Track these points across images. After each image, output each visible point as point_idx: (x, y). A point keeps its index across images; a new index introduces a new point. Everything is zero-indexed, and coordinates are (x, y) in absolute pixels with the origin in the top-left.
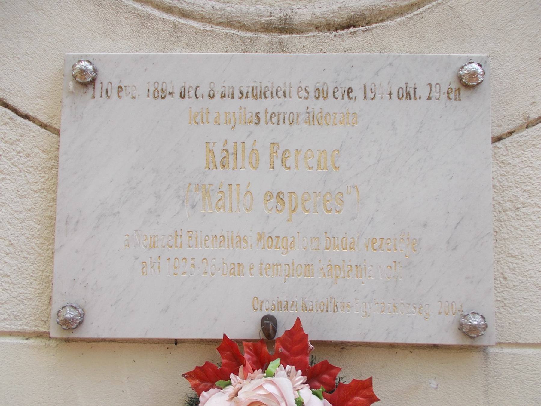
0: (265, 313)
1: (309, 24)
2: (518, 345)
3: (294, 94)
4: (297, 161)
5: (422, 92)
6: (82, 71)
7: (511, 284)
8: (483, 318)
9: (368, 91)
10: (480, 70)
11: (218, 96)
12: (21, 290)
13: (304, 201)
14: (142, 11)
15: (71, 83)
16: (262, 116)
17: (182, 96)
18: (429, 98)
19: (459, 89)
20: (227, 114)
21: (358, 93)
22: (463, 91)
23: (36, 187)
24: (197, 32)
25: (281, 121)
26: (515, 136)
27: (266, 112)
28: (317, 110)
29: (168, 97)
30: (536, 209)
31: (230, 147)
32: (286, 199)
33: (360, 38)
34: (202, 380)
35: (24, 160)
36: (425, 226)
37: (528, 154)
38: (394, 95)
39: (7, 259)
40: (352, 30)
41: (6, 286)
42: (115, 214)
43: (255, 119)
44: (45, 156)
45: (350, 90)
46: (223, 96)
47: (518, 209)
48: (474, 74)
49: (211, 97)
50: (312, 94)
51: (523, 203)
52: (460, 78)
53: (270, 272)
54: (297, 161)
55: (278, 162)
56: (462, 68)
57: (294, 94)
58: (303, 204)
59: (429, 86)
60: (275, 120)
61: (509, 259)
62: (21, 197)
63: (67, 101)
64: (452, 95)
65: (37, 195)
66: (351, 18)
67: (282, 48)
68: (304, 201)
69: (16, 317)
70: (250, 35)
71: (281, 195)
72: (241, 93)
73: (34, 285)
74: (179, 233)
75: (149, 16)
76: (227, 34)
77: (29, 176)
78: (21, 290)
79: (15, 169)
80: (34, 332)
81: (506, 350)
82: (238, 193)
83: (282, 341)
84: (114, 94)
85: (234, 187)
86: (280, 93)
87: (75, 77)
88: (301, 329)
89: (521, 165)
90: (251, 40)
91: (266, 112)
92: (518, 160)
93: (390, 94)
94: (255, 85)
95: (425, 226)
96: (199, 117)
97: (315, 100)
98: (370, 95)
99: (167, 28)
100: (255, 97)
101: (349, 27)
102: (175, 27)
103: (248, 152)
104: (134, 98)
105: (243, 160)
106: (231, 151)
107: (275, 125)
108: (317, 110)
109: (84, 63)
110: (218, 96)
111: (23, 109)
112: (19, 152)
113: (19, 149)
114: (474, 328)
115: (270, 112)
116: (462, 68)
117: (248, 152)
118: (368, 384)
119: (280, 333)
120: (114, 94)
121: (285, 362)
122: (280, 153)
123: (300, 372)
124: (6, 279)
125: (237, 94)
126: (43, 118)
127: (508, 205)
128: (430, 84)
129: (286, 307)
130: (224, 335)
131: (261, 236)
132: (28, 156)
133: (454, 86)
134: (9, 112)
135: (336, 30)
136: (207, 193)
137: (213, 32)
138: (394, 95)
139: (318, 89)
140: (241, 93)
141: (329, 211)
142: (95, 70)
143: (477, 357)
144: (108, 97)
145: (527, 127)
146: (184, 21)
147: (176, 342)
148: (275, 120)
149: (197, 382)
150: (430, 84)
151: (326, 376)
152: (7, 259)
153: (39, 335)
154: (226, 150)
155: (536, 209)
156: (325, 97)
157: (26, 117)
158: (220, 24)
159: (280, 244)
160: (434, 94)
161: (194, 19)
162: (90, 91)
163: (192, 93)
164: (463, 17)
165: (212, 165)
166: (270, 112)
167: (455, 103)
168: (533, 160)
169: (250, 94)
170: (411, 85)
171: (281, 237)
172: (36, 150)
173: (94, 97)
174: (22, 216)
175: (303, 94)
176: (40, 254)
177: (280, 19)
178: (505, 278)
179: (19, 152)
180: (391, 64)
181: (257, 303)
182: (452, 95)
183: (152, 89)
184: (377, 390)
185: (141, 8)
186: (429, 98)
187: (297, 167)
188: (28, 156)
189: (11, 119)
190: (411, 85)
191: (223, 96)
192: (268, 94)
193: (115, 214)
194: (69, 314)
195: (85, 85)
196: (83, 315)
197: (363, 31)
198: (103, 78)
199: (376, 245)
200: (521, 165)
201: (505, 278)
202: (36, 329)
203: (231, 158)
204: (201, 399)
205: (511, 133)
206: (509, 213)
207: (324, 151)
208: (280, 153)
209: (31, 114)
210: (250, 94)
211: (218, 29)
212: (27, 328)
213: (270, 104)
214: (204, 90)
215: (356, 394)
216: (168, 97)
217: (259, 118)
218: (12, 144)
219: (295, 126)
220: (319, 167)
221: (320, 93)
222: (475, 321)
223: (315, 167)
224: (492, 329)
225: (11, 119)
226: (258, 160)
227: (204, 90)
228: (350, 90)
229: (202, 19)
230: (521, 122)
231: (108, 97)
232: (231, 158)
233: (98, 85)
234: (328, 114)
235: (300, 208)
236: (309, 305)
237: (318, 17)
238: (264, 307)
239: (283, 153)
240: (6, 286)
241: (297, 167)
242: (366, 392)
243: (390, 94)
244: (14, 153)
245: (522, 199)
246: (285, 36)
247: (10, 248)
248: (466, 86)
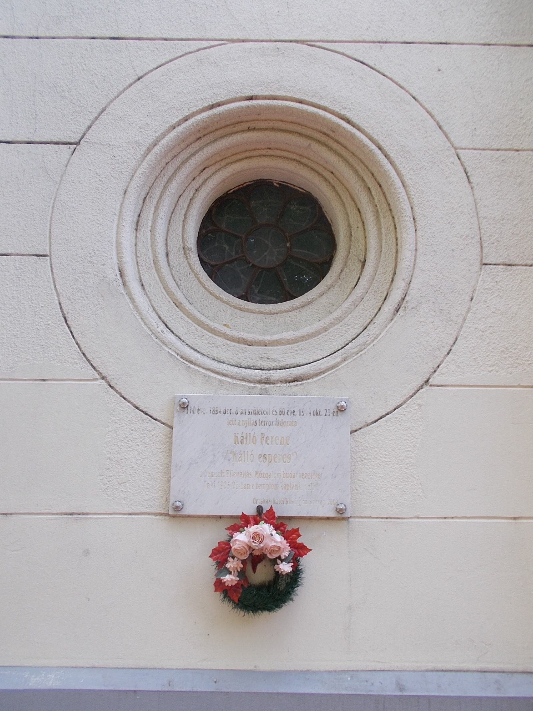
0: (259, 505)
1: (277, 381)
2: (362, 517)
3: (271, 413)
4: (272, 441)
5: (323, 413)
6: (184, 403)
7: (359, 492)
8: (345, 505)
9: (301, 412)
10: (345, 404)
11: (239, 413)
12: (154, 495)
13: (275, 458)
14: (206, 374)
15: (178, 407)
16: (258, 422)
17: (225, 413)
18: (326, 415)
19: (337, 412)
20: (243, 421)
21: (297, 413)
22: (339, 412)
23: (160, 450)
24: (230, 383)
25: (266, 424)
26: (362, 430)
27: (259, 421)
28: (280, 420)
29: (219, 413)
30: (369, 461)
31: (244, 435)
32: (267, 457)
33: (299, 387)
34: (233, 530)
35: (155, 438)
36: (323, 468)
37: (367, 437)
38: (312, 414)
39: (148, 481)
40: (296, 383)
41: (147, 493)
42: (196, 463)
43: (255, 424)
44: (164, 437)
45: (294, 412)
46: (241, 414)
47: (362, 461)
48: (342, 406)
49: (237, 414)
50: (278, 413)
51: (364, 458)
52: (338, 407)
53: (260, 487)
54: (272, 441)
55: (264, 442)
56: (338, 403)
57: (271, 413)
58: (274, 459)
59: (325, 411)
60: (263, 424)
61: (359, 482)
62: (154, 454)
63: (176, 415)
64: (335, 414)
65: (161, 454)
66: (295, 378)
67: (266, 392)
68: (275, 458)
69: (151, 507)
70: (252, 385)
71: (265, 456)
72: (249, 412)
73: (159, 493)
74: (223, 471)
75: (209, 376)
76: (242, 385)
77: (157, 445)
78: (154, 495)
79: (151, 442)
80: (160, 513)
81: (357, 520)
82: (247, 455)
83: (265, 515)
84: (196, 412)
85: (246, 452)
86: (265, 413)
87: (180, 405)
88: (273, 510)
89: (364, 442)
90: (253, 387)
91: (259, 421)
92: (363, 440)
93: (310, 413)
94: (255, 409)
95: (323, 468)
96: (232, 422)
97: (279, 416)
98: (302, 414)
99: (217, 382)
100: (255, 414)
101: (294, 381)
102: (221, 381)
103: (252, 437)
104: (204, 414)
105: (250, 440)
106: (245, 437)
107: (266, 415)
108: (280, 420)
109: (184, 399)
110: (239, 413)
111: (154, 417)
112: (153, 435)
113: (153, 434)
114: (341, 509)
115: (261, 420)
116: (338, 403)
117: (252, 437)
118: (297, 530)
119: (264, 512)
120: (196, 412)
121: (266, 522)
122: (265, 438)
123: (272, 526)
124: (147, 490)
125: (247, 413)
126: (163, 421)
127: (358, 459)
128: (326, 410)
129: (267, 502)
130: (243, 513)
131: (257, 473)
132: (157, 437)
133: (336, 410)
134: (149, 417)
135: (289, 382)
136: (234, 454)
137: (237, 384)
138: (312, 414)
139: (281, 411)
140: (249, 412)
141: (285, 462)
142: (188, 402)
143: (345, 522)
144: (193, 413)
145: (367, 426)
146: (223, 378)
147: (221, 517)
148: (263, 424)
149: (231, 531)
150: (326, 410)
151: (282, 528)
152: (148, 481)
153: (161, 514)
154: (243, 436)
155: (369, 461)
156: (284, 414)
157: (156, 420)
158: (240, 380)
159: (265, 476)
160: (328, 414)
161: (228, 377)
162: (186, 410)
163: (229, 412)
164: (341, 379)
165: (237, 443)
166: (261, 420)
167: (335, 417)
168: (368, 440)
169: (253, 413)
170: (318, 410)
171: (265, 473)
172: (160, 434)
173: (187, 413)
174: (154, 463)
175: (275, 413)
176: (162, 480)
177: (265, 378)
178: (357, 490)
179: (153, 435)
180: (310, 401)
181: (255, 500)
182: (335, 414)
183: (212, 410)
184: (301, 532)
185: (206, 372)
186: (326, 415)
187: (272, 444)
188: (157, 437)
189: (150, 420)
190: (318, 410)
191: (241, 414)
192: (260, 413)
193: (196, 463)
194: (178, 504)
195: (184, 408)
196: (183, 505)
197: (300, 385)
198: (192, 405)
199: (304, 477)
200: (364, 442)
201: (357, 490)
202: (160, 512)
203: (245, 440)
204: (234, 536)
205: (361, 428)
206: (359, 462)
207: (283, 437)
208: (265, 438)
209: (158, 418)
210: (253, 413)
211: (239, 382)
212: (157, 511)
213: (261, 417)
214: (233, 411)
215: (293, 534)
216: (219, 413)
217: (256, 423)
218: (150, 431)
219: (271, 427)
220: (281, 444)
221: (282, 413)
222: (342, 506)
223: (279, 443)
224: (349, 510)
225: (150, 420)
226: (256, 441)
227: (233, 411)
228: (294, 412)
229: (232, 377)
230: (364, 424)
231: (193, 413)
232: (245, 440)
233: (189, 407)
234: (285, 422)
235: (273, 461)
236: (276, 501)
237: (281, 378)
238: (258, 502)
239: (266, 438)
240: (147, 493)
241: (272, 444)
242: (297, 533)
243: (310, 413)
244: (151, 435)
245: (364, 457)
246: (267, 386)
247: (149, 477)
248: (340, 410)
